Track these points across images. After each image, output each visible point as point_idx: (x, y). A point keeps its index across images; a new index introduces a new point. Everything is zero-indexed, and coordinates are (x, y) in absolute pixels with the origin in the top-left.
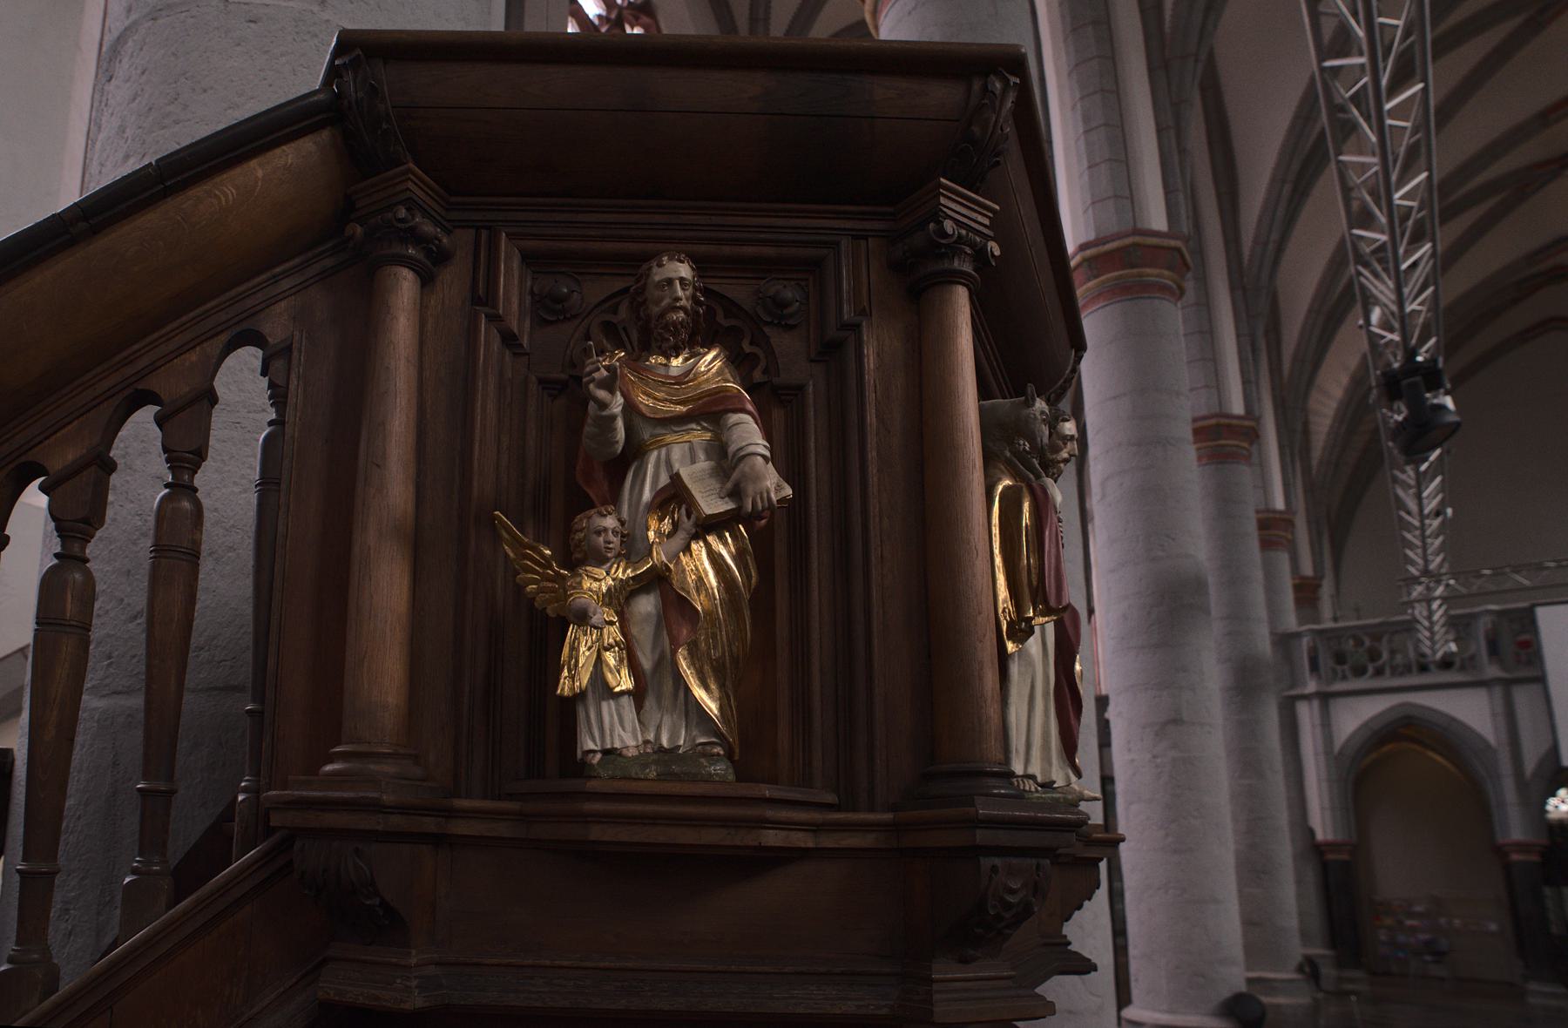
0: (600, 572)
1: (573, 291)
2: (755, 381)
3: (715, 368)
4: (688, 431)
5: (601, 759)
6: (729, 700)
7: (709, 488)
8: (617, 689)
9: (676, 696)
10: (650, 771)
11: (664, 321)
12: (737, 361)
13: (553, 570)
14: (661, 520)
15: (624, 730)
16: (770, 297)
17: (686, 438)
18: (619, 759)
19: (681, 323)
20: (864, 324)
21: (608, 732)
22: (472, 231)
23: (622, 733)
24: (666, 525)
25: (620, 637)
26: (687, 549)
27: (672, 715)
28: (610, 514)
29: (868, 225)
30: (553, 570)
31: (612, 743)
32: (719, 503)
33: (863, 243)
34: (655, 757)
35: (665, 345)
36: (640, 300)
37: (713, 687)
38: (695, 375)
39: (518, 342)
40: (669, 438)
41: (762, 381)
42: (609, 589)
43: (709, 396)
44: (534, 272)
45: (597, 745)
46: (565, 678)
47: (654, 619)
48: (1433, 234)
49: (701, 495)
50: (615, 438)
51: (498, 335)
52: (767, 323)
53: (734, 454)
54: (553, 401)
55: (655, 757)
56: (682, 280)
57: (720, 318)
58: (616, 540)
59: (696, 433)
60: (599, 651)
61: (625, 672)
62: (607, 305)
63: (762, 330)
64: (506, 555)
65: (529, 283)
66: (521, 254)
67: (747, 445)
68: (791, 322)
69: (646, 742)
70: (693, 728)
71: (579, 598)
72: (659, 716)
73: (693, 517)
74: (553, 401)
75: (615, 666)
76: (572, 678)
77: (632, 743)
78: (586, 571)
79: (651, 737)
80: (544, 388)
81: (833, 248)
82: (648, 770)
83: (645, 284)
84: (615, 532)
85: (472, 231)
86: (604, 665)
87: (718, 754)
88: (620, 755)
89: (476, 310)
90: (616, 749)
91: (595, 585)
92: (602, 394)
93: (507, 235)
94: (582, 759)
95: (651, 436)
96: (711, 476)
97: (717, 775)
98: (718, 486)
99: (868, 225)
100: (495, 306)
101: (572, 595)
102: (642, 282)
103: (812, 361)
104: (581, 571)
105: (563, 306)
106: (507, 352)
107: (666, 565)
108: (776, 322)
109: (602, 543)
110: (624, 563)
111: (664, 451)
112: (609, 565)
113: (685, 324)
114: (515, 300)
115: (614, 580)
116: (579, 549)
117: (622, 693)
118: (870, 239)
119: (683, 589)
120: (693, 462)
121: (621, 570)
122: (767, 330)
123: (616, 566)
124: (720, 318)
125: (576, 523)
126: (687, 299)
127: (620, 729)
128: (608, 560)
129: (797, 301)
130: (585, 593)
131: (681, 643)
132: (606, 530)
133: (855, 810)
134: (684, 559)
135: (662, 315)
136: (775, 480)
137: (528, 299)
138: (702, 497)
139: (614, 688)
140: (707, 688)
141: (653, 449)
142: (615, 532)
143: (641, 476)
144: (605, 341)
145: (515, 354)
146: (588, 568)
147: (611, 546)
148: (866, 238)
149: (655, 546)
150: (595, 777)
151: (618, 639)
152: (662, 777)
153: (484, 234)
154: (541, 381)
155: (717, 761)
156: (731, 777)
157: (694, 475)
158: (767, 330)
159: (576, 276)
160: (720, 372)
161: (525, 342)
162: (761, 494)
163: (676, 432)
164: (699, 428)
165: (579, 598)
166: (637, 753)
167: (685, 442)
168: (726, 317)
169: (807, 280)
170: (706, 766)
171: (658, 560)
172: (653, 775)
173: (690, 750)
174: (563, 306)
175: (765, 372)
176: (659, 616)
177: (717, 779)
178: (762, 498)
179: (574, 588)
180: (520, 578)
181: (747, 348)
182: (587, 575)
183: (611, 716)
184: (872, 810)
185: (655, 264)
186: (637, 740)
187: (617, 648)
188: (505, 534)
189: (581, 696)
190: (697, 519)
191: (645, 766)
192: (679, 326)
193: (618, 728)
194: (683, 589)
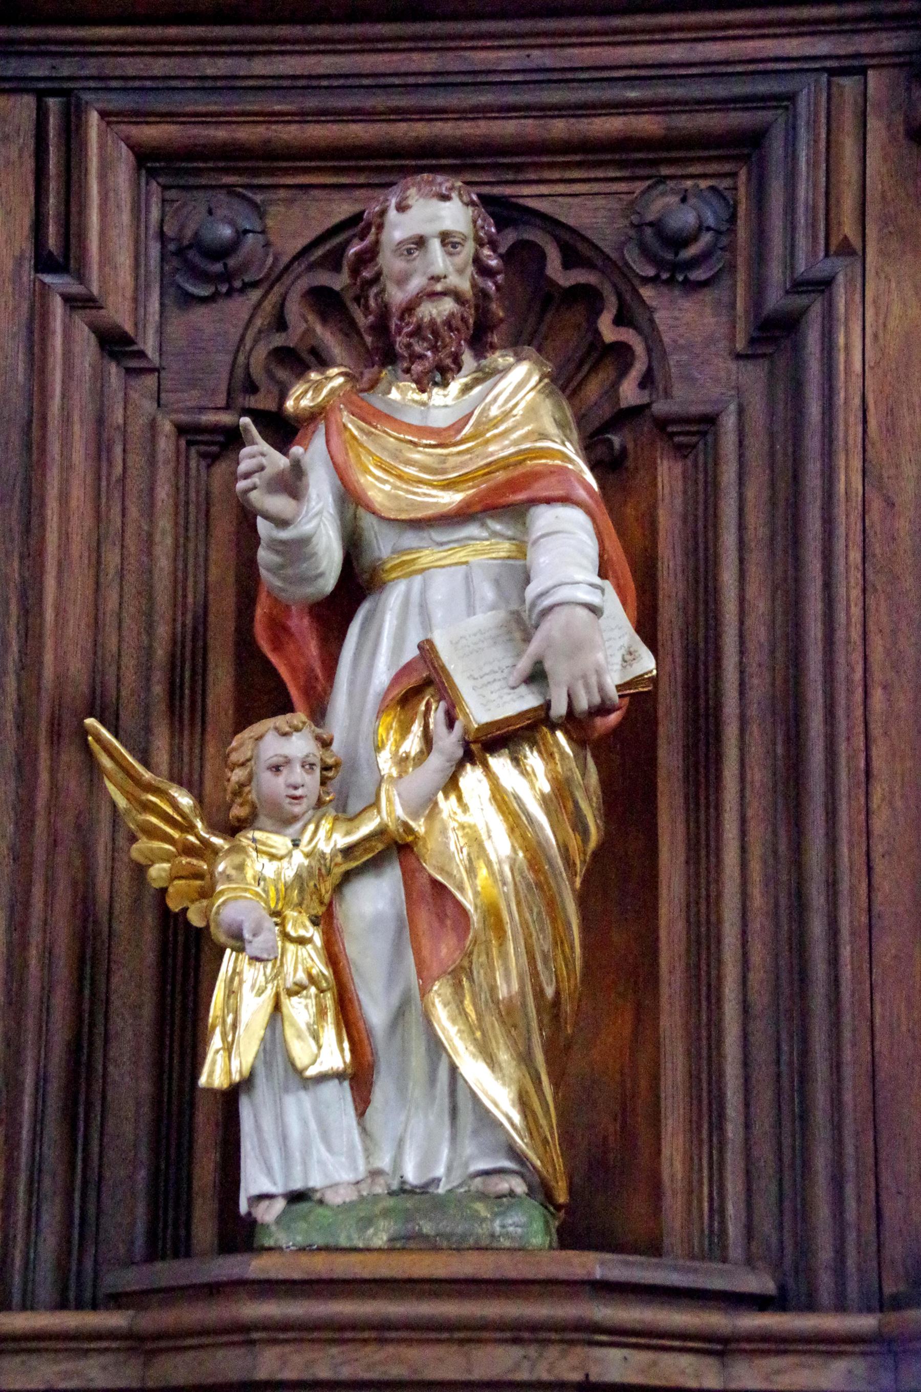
0: (280, 842)
1: (246, 232)
2: (624, 404)
3: (523, 405)
4: (463, 542)
5: (284, 1212)
6: (537, 1082)
7: (487, 669)
8: (311, 1072)
9: (432, 1079)
10: (375, 1234)
11: (415, 320)
12: (681, 272)
13: (198, 837)
14: (405, 730)
15: (329, 1148)
16: (651, 224)
17: (461, 555)
18: (320, 1210)
19: (448, 323)
20: (841, 278)
21: (297, 1155)
22: (29, 101)
23: (325, 1154)
24: (413, 744)
25: (320, 967)
26: (451, 784)
27: (426, 1116)
28: (297, 730)
29: (864, 44)
30: (198, 837)
31: (306, 1174)
32: (507, 698)
33: (848, 83)
34: (391, 1202)
35: (417, 368)
36: (366, 274)
37: (504, 1056)
38: (478, 423)
39: (135, 348)
40: (427, 557)
41: (639, 402)
42: (298, 876)
43: (505, 468)
44: (165, 188)
45: (275, 1184)
46: (217, 1052)
47: (391, 926)
48: (137, 900)
49: (472, 683)
50: (317, 568)
51: (93, 336)
52: (646, 280)
53: (533, 605)
54: (209, 467)
55: (391, 1202)
56: (445, 238)
57: (554, 266)
58: (312, 781)
59: (479, 545)
60: (277, 996)
61: (329, 1033)
62: (320, 252)
63: (637, 291)
64: (114, 805)
65: (155, 214)
66: (135, 153)
67: (555, 587)
68: (699, 275)
69: (375, 1174)
70: (467, 1142)
71: (236, 899)
72: (403, 1118)
73: (458, 726)
74: (209, 467)
75: (309, 1026)
76: (228, 1049)
77: (346, 1176)
78: (254, 840)
79: (384, 1162)
80: (189, 443)
81: (786, 108)
82: (371, 1231)
83: (377, 242)
84: (308, 766)
85: (29, 101)
86: (287, 1024)
87: (511, 1194)
88: (321, 1202)
89: (43, 284)
90: (314, 1190)
91: (270, 869)
92: (278, 504)
93: (103, 114)
94: (249, 1214)
95: (393, 553)
96: (495, 641)
97: (507, 1235)
98: (508, 662)
99: (864, 44)
100: (81, 278)
101: (222, 893)
102: (371, 238)
103: (739, 357)
104: (245, 842)
105: (225, 265)
106: (113, 368)
107: (406, 825)
108: (665, 276)
109: (283, 786)
110: (330, 819)
111: (418, 580)
112: (298, 826)
113: (456, 323)
114: (124, 259)
115: (307, 855)
116: (239, 800)
117: (322, 1078)
118: (870, 73)
119: (441, 870)
120: (471, 610)
121: (322, 833)
122: (647, 293)
123: (311, 827)
124: (554, 266)
125: (234, 749)
126: (460, 272)
127: (322, 1149)
128: (295, 819)
129: (709, 229)
130: (246, 890)
131: (435, 973)
132: (288, 761)
133: (810, 1306)
134: (447, 805)
135: (409, 309)
136: (625, 641)
137: (155, 249)
138: (474, 688)
139: (306, 1068)
140: (492, 1061)
141: (398, 578)
142: (308, 766)
143: (372, 634)
144: (319, 329)
145: (129, 371)
146: (258, 835)
147: (298, 793)
148: (862, 71)
149: (384, 787)
150: (270, 1249)
151: (314, 972)
152: (398, 1245)
153: (53, 103)
154: (182, 430)
155: (509, 1207)
156: (538, 1239)
157: (464, 642)
158: (647, 293)
159: (249, 194)
160: (532, 412)
161: (149, 345)
162: (584, 677)
163: (442, 544)
164: (485, 534)
165: (236, 899)
166: (354, 1197)
167: (456, 564)
168: (567, 264)
169: (734, 175)
170: (484, 1219)
171: (389, 814)
172: (380, 1240)
173: (460, 1185)
174: (225, 265)
175: (647, 381)
176: (399, 919)
177: (507, 1244)
178: (587, 686)
179: (229, 878)
180: (140, 851)
181: (609, 332)
182: (257, 850)
183: (305, 1123)
184: (841, 1307)
185: (393, 201)
186: (356, 1169)
187: (313, 990)
188: (106, 762)
189: (245, 1085)
190: (466, 731)
191: (367, 1222)
192: (444, 331)
193: (319, 1149)
194: (441, 870)
